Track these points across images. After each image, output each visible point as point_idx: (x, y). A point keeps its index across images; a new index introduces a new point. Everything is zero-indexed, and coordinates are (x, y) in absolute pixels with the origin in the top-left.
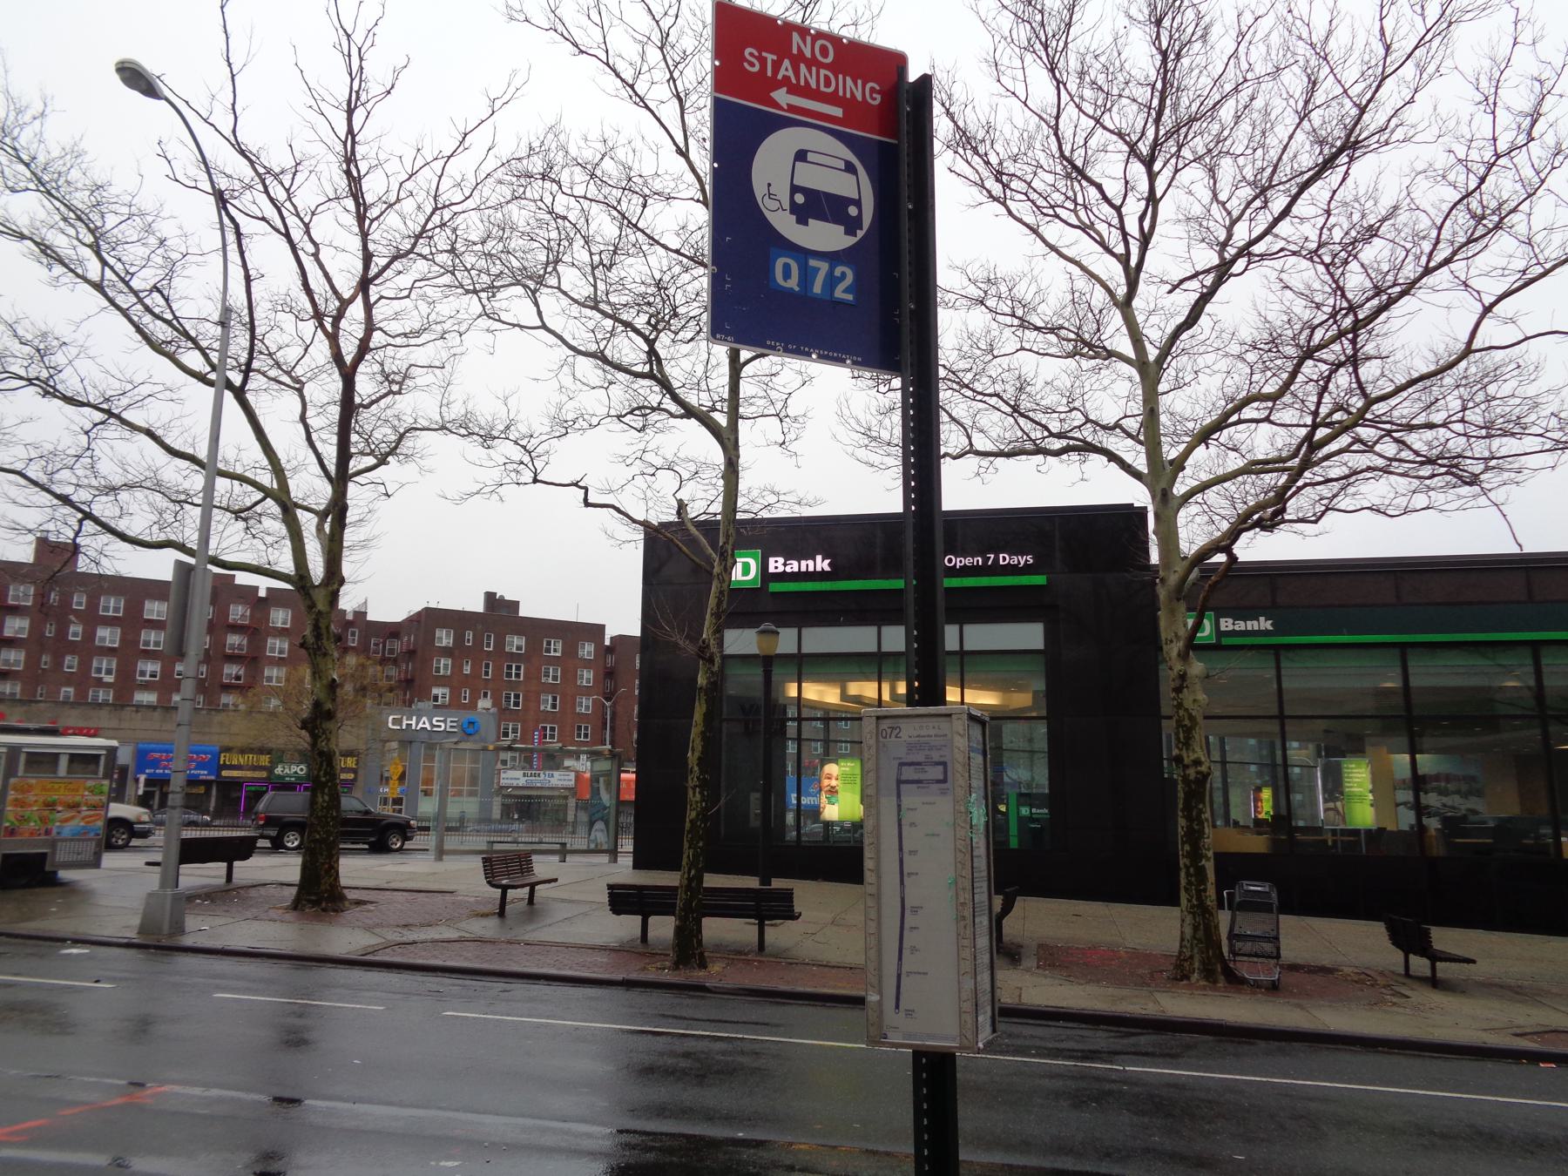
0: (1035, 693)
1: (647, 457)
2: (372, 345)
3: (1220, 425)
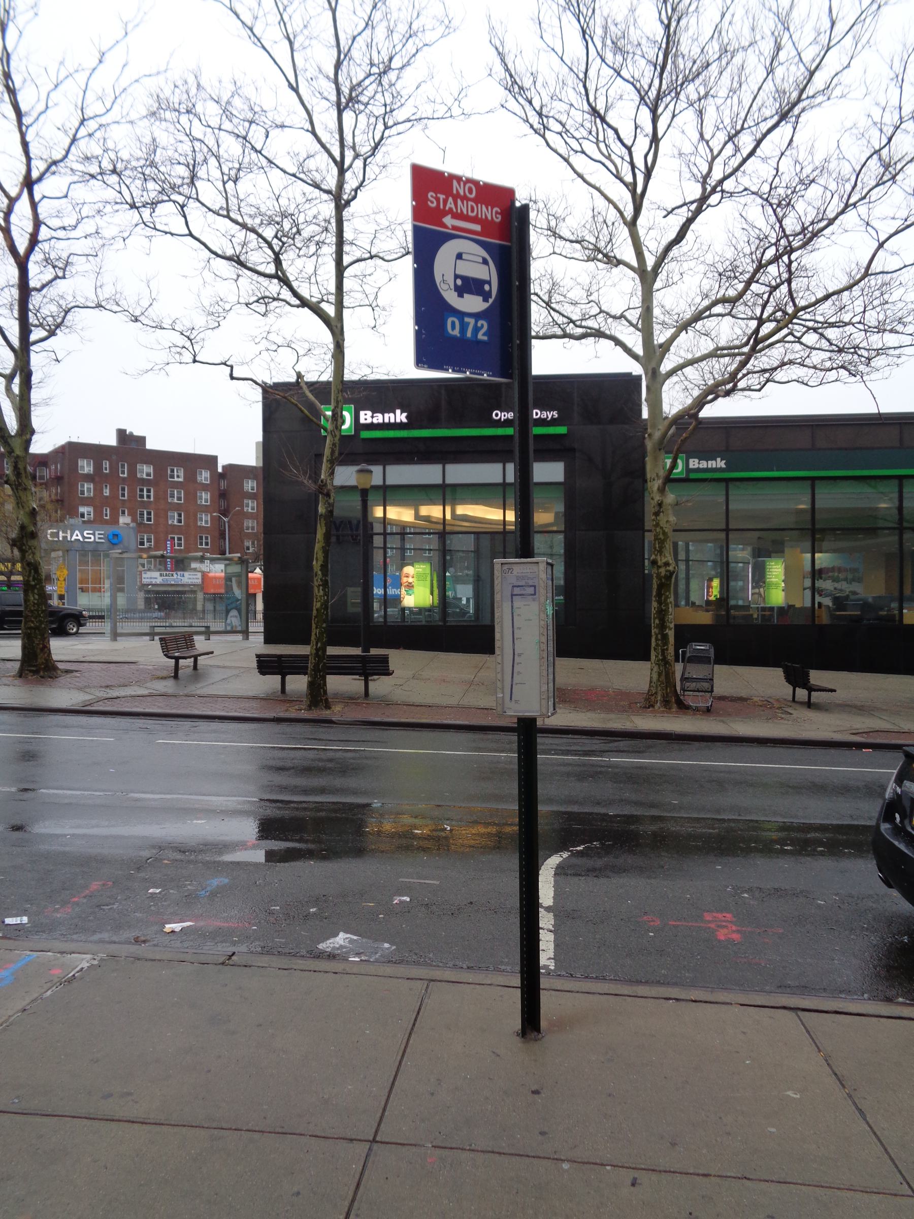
0: (557, 514)
1: (270, 337)
2: (40, 238)
3: (698, 317)
